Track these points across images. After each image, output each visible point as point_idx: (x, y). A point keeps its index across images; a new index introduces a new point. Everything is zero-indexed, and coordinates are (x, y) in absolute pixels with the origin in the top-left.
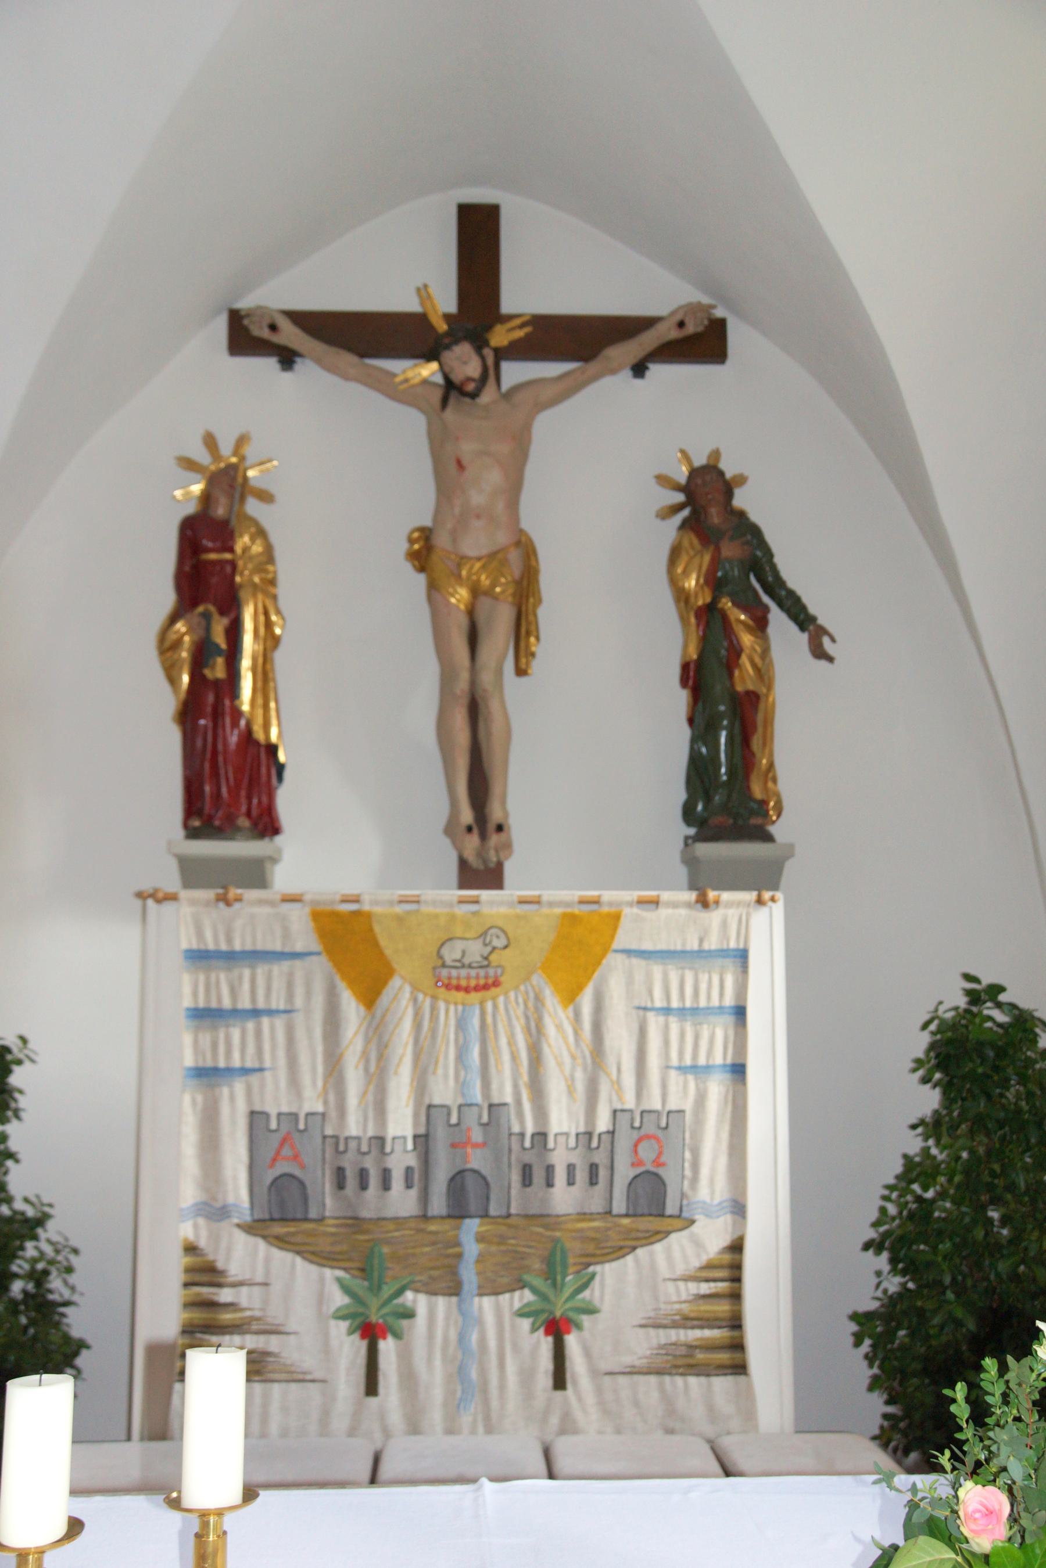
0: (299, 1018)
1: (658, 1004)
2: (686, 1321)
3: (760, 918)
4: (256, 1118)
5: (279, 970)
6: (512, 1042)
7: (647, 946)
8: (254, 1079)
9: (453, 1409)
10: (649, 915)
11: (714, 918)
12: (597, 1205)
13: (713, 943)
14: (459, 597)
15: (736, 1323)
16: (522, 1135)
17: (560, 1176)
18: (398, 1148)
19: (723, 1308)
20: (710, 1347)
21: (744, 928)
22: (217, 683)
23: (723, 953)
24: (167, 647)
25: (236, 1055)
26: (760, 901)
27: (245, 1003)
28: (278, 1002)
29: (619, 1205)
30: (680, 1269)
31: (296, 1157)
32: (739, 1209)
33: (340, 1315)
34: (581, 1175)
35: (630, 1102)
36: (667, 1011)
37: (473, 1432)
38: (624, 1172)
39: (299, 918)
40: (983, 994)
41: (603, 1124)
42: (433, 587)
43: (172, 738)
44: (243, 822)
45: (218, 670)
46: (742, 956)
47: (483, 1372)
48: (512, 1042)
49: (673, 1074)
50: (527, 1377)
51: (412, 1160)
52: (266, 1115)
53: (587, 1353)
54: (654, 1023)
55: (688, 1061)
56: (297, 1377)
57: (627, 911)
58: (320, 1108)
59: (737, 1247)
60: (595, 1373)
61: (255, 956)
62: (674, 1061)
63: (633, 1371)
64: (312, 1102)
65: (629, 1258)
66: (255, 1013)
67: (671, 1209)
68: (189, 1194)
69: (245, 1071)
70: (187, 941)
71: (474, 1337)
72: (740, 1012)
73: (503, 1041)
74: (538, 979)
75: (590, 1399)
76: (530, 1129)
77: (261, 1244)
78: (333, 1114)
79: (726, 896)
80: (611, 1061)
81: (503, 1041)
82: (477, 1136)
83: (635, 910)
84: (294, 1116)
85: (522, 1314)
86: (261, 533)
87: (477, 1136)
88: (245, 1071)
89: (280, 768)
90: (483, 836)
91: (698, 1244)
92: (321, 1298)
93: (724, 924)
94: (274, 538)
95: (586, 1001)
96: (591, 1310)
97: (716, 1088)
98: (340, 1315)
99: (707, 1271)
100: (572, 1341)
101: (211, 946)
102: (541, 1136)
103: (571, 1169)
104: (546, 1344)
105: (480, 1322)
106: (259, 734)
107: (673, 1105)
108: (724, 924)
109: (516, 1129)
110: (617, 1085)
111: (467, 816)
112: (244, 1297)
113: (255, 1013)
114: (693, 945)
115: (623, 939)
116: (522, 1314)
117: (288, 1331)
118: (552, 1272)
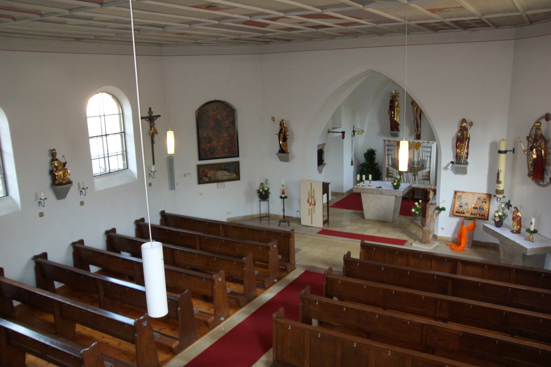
1: (424, 150)
2: (425, 176)
3: (433, 144)
4: (392, 158)
5: (393, 147)
7: (423, 146)
9: (406, 181)
10: (424, 144)
11: (429, 144)
12: (418, 167)
13: (429, 146)
14: (415, 109)
15: (429, 177)
17: (415, 164)
19: (428, 176)
20: (427, 178)
21: (432, 145)
22: (393, 118)
23: (430, 147)
24: (389, 113)
26: (433, 143)
27: (391, 149)
28: (393, 149)
29: (420, 167)
30: (425, 172)
32: (430, 168)
33: (398, 173)
34: (417, 164)
35: (421, 158)
36: (425, 151)
37: (406, 182)
38: (421, 164)
39: (395, 143)
40: (538, 136)
41: (419, 160)
42: (413, 108)
43: (389, 121)
44: (395, 129)
45: (393, 116)
46: (431, 147)
47: (409, 179)
49: (425, 157)
50: (412, 179)
53: (417, 178)
54: (424, 153)
55: (426, 155)
56: (421, 180)
57: (422, 143)
59: (430, 171)
60: (418, 180)
61: (392, 145)
62: (425, 155)
63: (421, 180)
65: (421, 171)
66: (392, 150)
67: (424, 167)
68: (387, 163)
69: (391, 154)
70: (386, 144)
71: (408, 176)
72: (431, 152)
74: (414, 148)
75: (417, 181)
76: (413, 160)
77: (392, 168)
79: (430, 142)
80: (420, 155)
83: (422, 143)
85: (412, 174)
86: (397, 101)
88: (391, 154)
89: (399, 124)
90: (418, 131)
91: (426, 170)
92: (397, 172)
93: (430, 145)
94: (399, 102)
95: (418, 151)
96: (418, 175)
97: (429, 158)
98: (398, 173)
99: (427, 173)
100: (416, 177)
101: (388, 144)
102: (414, 161)
103: (416, 164)
104: (414, 177)
105: (409, 175)
106: (397, 121)
107: (425, 159)
108: (430, 145)
110: (420, 158)
111: (416, 129)
112: (391, 172)
113: (392, 150)
114: (427, 146)
115: (421, 145)
116: (412, 174)
117: (491, 199)
118: (414, 171)
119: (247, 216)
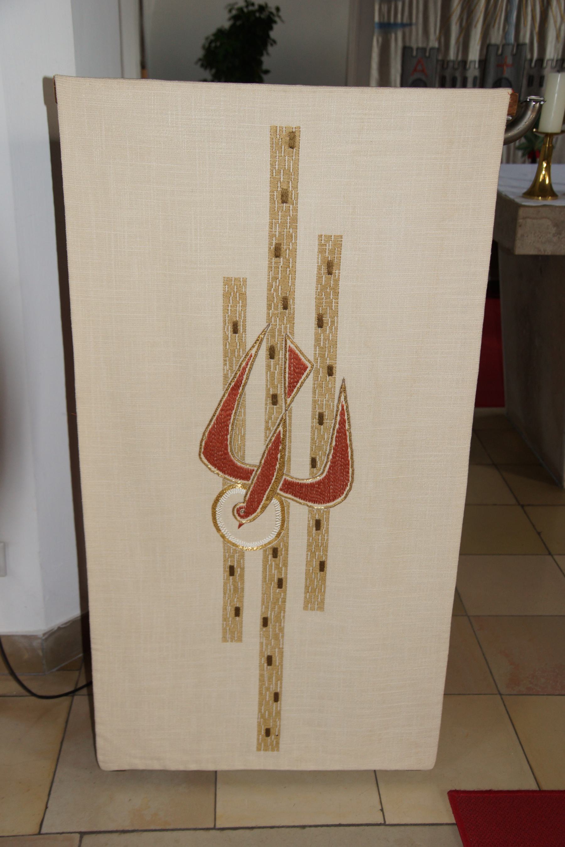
0: (414, 28)
4: (406, 50)
6: (533, 11)
8: (407, 30)
16: (531, 60)
18: (472, 66)
25: (399, 16)
31: (423, 71)
48: (533, 11)
51: (477, 73)
52: (411, 49)
58: (436, 45)
64: (433, 43)
69: (403, 25)
73: (529, 9)
78: (443, 48)
81: (529, 9)
82: (509, 60)
84: (424, 50)
87: (509, 60)
102: (541, 60)
109: (529, 57)
119: (174, 828)
